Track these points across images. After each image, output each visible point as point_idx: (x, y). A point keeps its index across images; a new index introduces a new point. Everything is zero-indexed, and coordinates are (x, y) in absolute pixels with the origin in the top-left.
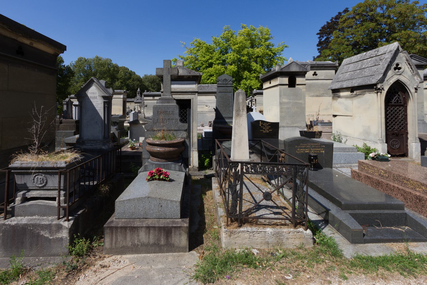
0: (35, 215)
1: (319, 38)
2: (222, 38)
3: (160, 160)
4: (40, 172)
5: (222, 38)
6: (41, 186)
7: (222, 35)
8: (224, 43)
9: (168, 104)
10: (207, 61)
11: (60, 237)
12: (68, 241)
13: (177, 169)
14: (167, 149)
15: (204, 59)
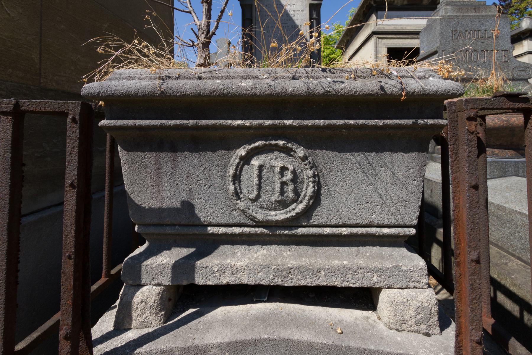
6: (280, 215)
9: (478, 14)
14: (259, 230)
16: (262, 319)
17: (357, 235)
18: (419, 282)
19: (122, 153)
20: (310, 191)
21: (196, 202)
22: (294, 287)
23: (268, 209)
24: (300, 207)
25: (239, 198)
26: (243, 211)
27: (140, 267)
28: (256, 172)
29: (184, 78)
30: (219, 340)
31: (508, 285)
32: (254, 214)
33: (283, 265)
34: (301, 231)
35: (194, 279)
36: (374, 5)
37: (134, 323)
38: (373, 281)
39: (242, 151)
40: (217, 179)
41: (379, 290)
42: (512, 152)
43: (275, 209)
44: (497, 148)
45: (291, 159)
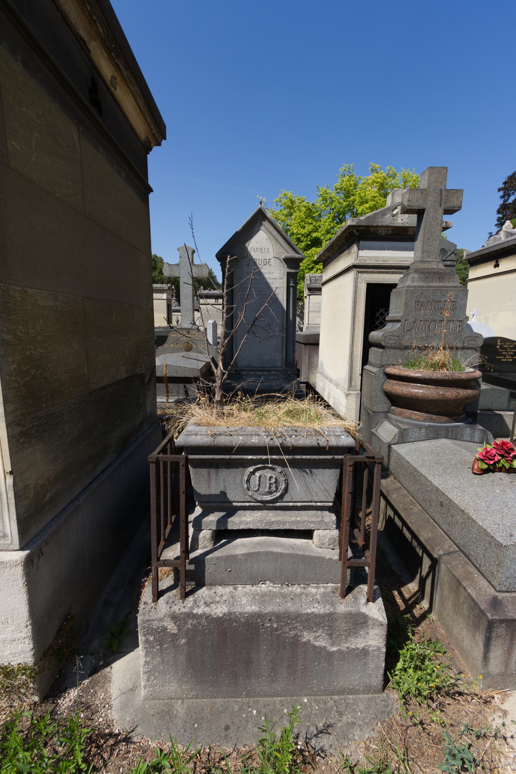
0: (264, 581)
1: (502, 197)
2: (339, 190)
3: (434, 417)
4: (266, 461)
5: (337, 189)
6: (269, 498)
7: (338, 185)
8: (341, 201)
9: (442, 284)
10: (308, 235)
11: (360, 646)
12: (383, 657)
13: (476, 439)
15: (303, 231)
16: (260, 544)
17: (305, 506)
18: (332, 527)
19: (191, 469)
20: (283, 487)
21: (228, 492)
22: (274, 530)
23: (263, 495)
24: (278, 494)
25: (249, 490)
26: (251, 496)
27: (201, 522)
28: (258, 479)
29: (224, 435)
30: (242, 552)
31: (408, 523)
32: (256, 497)
33: (269, 520)
34: (278, 504)
35: (227, 527)
36: (357, 234)
37: (200, 547)
38: (311, 526)
39: (251, 469)
40: (238, 481)
41: (314, 531)
42: (446, 418)
43: (266, 495)
44: (435, 415)
45: (274, 472)
